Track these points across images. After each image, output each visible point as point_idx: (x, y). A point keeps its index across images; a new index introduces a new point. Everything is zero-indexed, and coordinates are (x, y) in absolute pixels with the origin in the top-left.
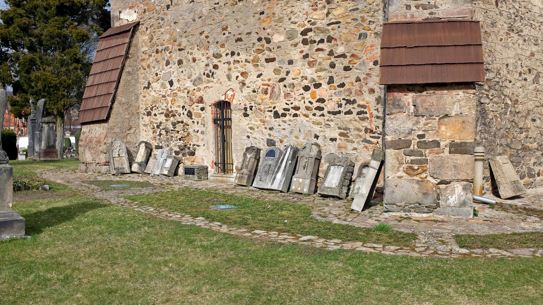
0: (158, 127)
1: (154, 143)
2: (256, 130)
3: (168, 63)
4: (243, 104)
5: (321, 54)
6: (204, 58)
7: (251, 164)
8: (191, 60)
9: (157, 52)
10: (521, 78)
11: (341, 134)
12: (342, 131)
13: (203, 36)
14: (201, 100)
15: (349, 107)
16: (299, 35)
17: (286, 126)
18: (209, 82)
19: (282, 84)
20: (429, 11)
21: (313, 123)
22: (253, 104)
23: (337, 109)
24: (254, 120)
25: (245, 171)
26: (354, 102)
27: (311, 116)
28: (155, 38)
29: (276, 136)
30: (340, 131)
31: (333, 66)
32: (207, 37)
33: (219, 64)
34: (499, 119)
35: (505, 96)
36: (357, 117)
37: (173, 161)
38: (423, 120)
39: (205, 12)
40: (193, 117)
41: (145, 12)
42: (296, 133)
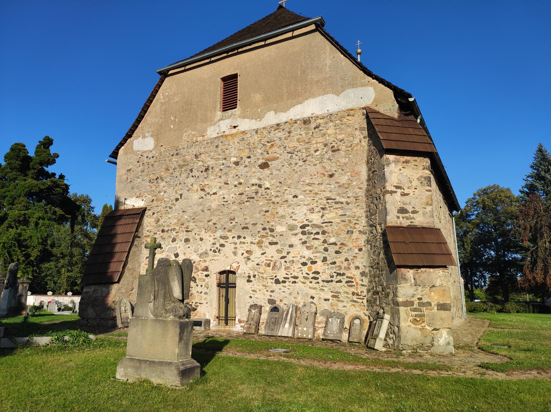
5: (316, 242)
6: (211, 239)
8: (198, 239)
9: (163, 231)
12: (334, 294)
13: (211, 223)
14: (206, 269)
15: (339, 278)
16: (299, 228)
19: (283, 260)
20: (410, 221)
21: (310, 288)
22: (256, 273)
24: (256, 284)
26: (344, 274)
30: (332, 294)
31: (326, 250)
33: (225, 244)
38: (420, 289)
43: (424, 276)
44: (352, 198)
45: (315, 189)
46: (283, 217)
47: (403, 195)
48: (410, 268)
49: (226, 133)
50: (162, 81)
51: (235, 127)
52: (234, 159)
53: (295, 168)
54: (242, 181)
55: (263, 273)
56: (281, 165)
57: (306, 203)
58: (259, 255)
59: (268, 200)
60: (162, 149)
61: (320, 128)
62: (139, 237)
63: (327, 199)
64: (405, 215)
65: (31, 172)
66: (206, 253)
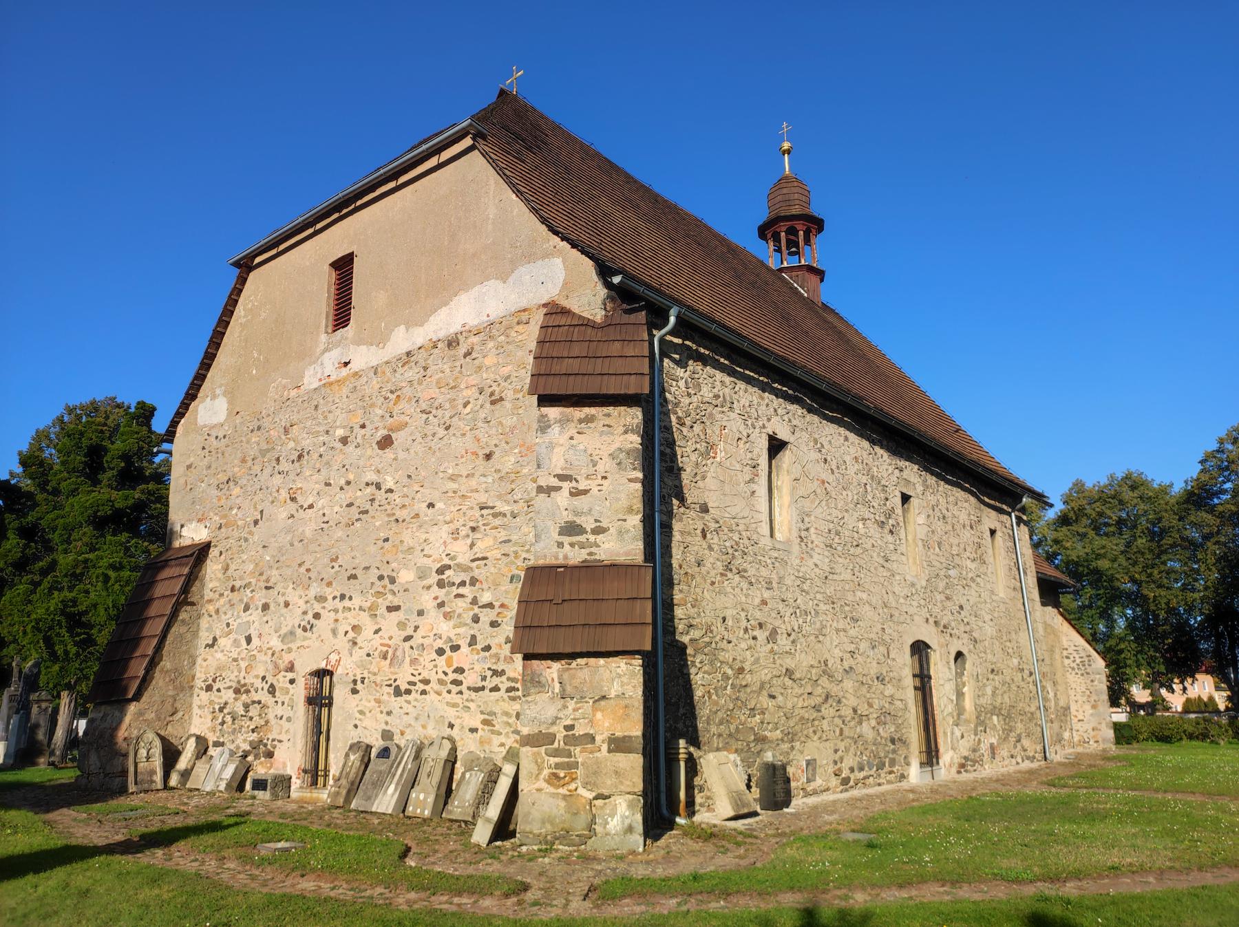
0: (221, 710)
1: (212, 738)
2: (368, 714)
3: (246, 608)
4: (351, 675)
5: (459, 601)
6: (301, 602)
7: (354, 770)
8: (282, 604)
9: (233, 589)
10: (747, 636)
11: (486, 722)
12: (486, 717)
13: (303, 570)
14: (291, 668)
15: (496, 681)
16: (434, 574)
17: (410, 709)
18: (305, 639)
19: (407, 644)
20: (588, 550)
21: (448, 703)
22: (366, 675)
23: (480, 684)
24: (366, 698)
25: (344, 782)
26: (503, 673)
27: (445, 694)
28: (233, 567)
29: (395, 725)
30: (483, 717)
31: (476, 619)
32: (308, 570)
33: (321, 611)
34: (714, 697)
35: (722, 662)
36: (506, 696)
37: (237, 768)
38: (571, 704)
39: (308, 533)
40: (277, 694)
41: (220, 528)
42: (423, 719)
43: (584, 674)
44: (521, 503)
45: (463, 488)
46: (410, 550)
47: (576, 493)
48: (552, 659)
49: (333, 378)
50: (242, 280)
51: (346, 364)
52: (340, 432)
53: (432, 444)
54: (351, 477)
55: (375, 674)
56: (410, 439)
57: (448, 518)
58: (371, 635)
59: (389, 515)
60: (238, 420)
61: (474, 355)
62: (193, 604)
63: (482, 508)
64: (575, 539)
65: (105, 477)
66: (292, 633)
